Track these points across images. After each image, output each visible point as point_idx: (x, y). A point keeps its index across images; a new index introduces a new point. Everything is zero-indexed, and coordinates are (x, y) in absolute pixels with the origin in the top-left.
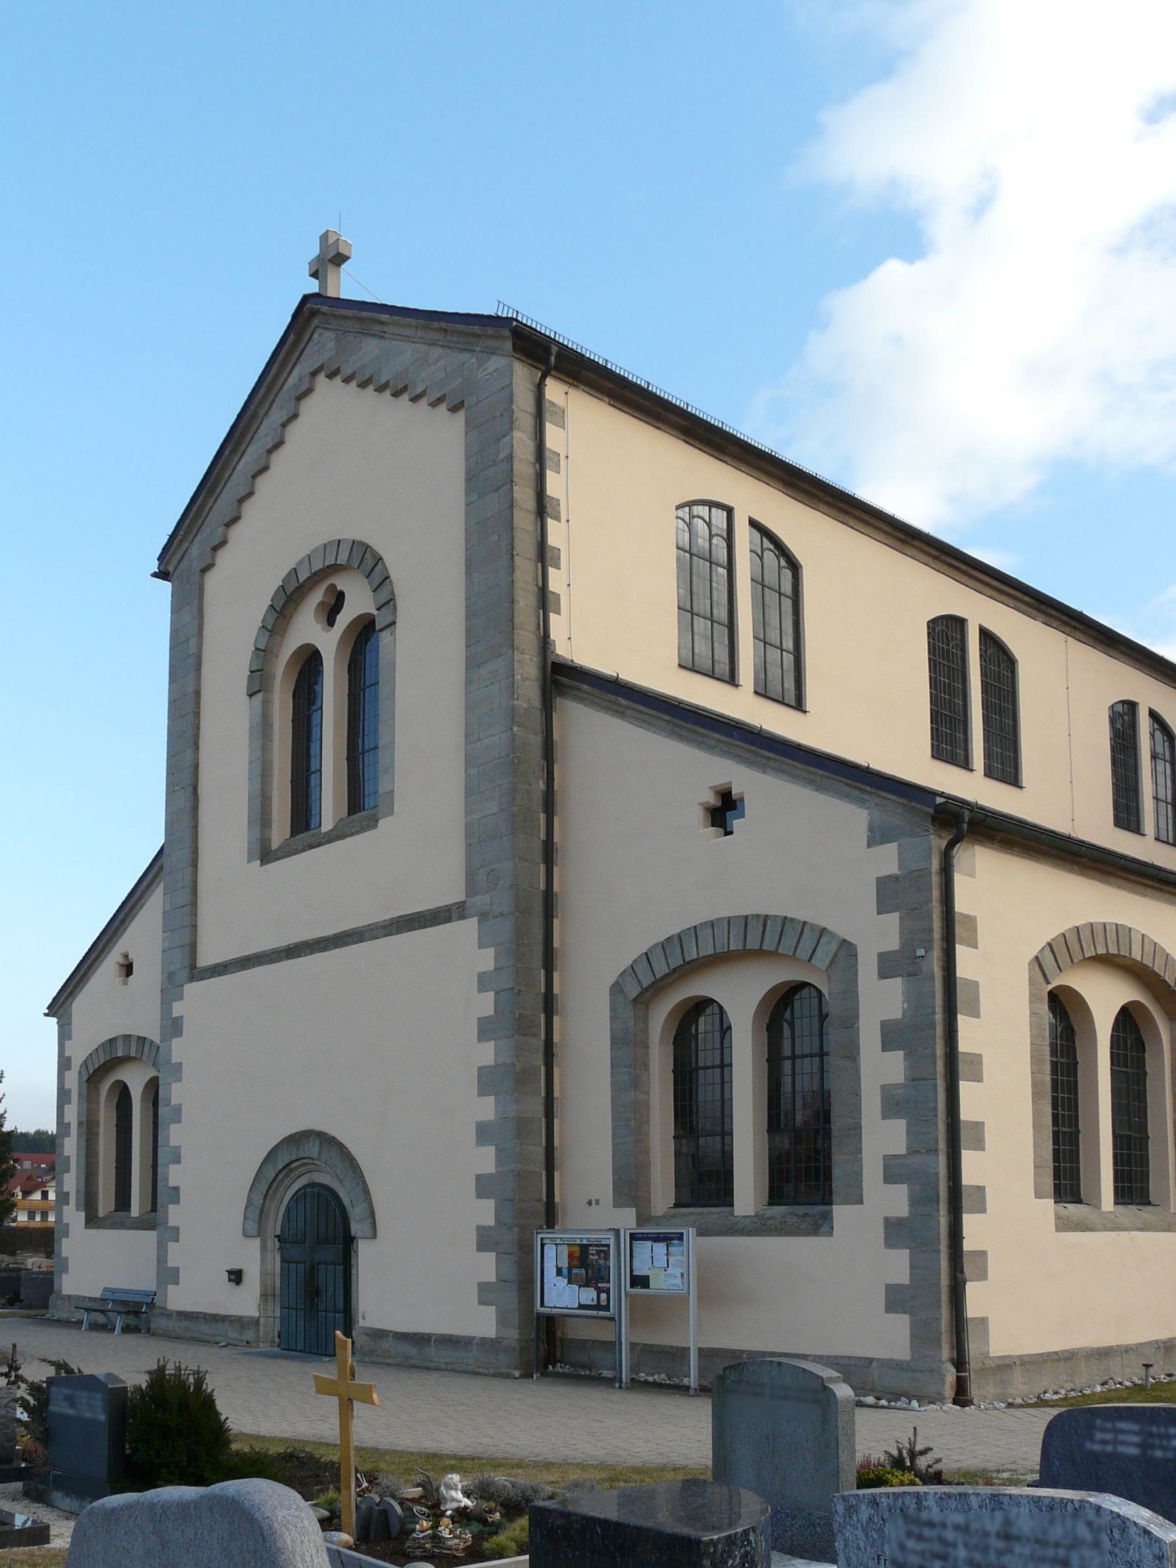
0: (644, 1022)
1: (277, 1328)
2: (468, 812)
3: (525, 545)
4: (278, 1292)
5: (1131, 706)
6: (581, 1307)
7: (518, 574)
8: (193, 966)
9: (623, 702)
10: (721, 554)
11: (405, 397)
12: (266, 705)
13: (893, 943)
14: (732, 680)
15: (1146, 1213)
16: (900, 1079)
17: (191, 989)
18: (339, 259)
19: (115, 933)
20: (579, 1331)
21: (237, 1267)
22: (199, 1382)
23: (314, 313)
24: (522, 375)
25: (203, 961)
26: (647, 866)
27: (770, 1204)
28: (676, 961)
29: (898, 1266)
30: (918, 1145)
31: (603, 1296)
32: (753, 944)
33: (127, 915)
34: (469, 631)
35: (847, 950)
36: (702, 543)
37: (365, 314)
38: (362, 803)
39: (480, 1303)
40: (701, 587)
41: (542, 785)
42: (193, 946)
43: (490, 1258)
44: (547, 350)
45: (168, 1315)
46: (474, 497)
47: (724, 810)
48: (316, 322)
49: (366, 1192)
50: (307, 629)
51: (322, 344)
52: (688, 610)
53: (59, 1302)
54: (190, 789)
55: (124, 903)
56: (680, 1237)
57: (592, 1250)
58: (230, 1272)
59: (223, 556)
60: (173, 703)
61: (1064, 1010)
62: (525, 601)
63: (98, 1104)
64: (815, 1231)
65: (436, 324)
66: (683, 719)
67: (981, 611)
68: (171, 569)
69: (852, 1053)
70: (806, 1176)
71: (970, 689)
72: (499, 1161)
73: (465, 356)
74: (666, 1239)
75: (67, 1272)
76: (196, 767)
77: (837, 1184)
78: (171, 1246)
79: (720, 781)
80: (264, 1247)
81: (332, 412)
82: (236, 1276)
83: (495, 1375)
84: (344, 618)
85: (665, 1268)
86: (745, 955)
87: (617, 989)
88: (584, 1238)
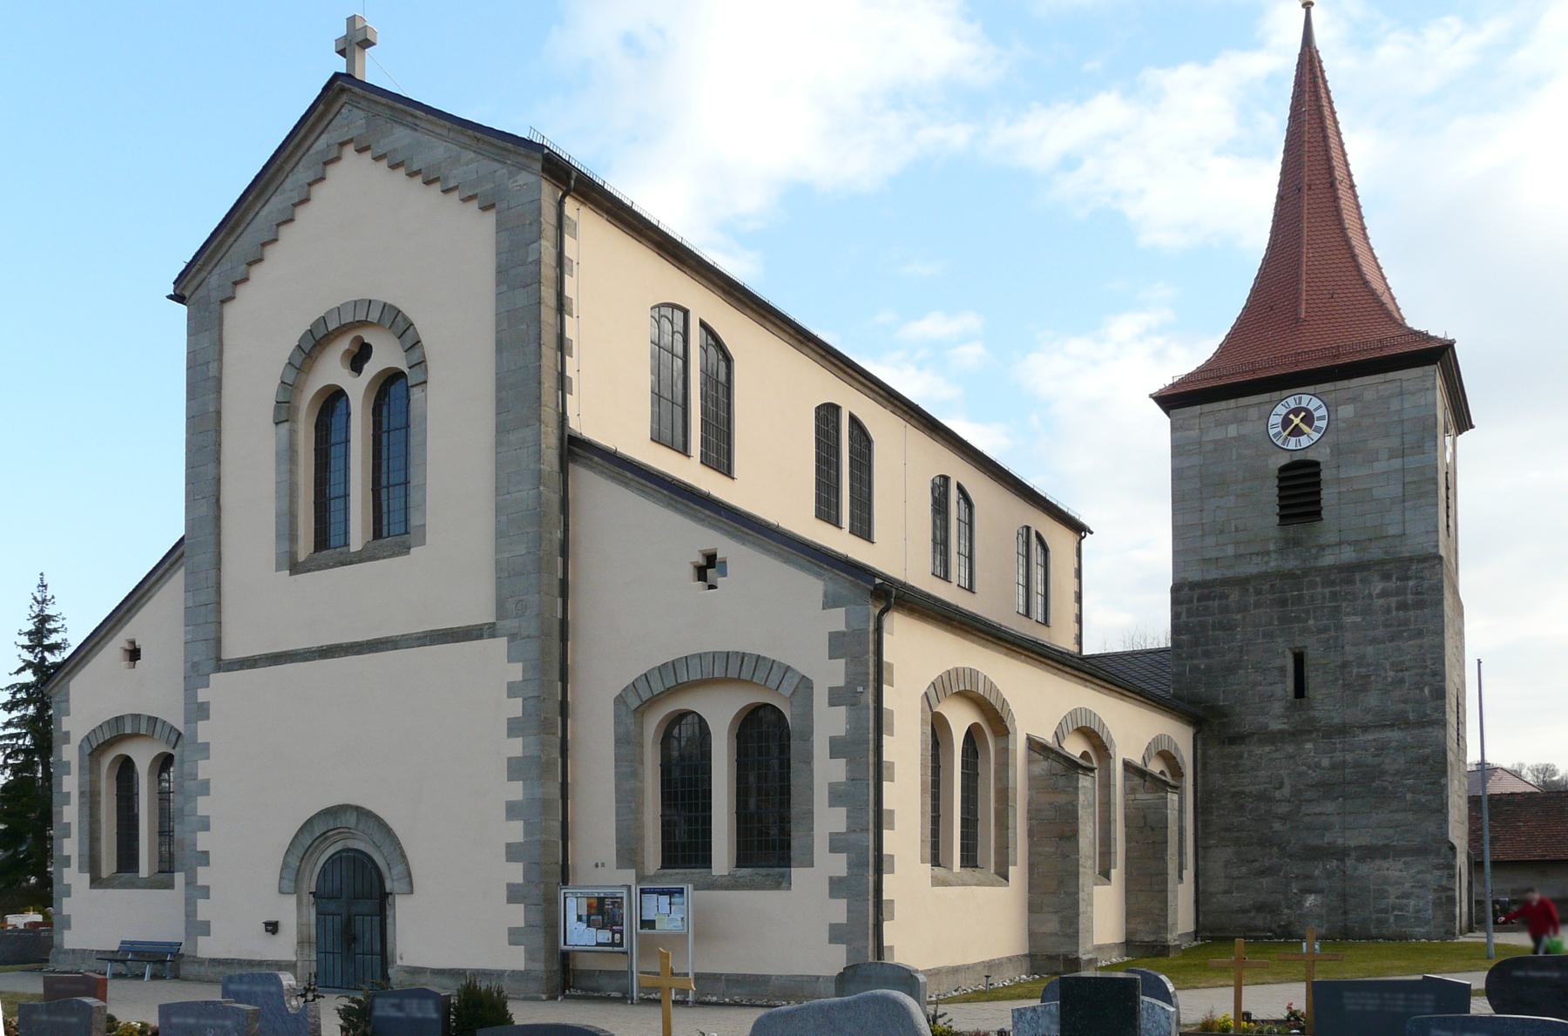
0: (640, 726)
1: (314, 969)
2: (498, 549)
3: (549, 337)
4: (313, 939)
5: (946, 479)
6: (598, 944)
7: (544, 360)
8: (219, 659)
9: (629, 475)
10: (679, 349)
11: (437, 187)
12: (293, 433)
13: (840, 681)
14: (685, 451)
15: (977, 873)
16: (844, 779)
17: (217, 679)
18: (366, 43)
19: (119, 621)
20: (582, 964)
21: (273, 919)
22: (499, 993)
23: (343, 90)
24: (548, 193)
25: (231, 652)
26: (644, 607)
27: (739, 865)
28: (671, 682)
29: (839, 911)
30: (855, 825)
31: (617, 936)
32: (733, 673)
33: (134, 605)
34: (499, 401)
35: (806, 684)
36: (667, 340)
37: (398, 105)
38: (393, 527)
39: (511, 943)
40: (665, 374)
41: (559, 535)
42: (218, 641)
43: (519, 909)
44: (569, 175)
45: (201, 962)
46: (505, 288)
47: (707, 568)
48: (344, 98)
49: (404, 856)
50: (332, 370)
51: (351, 120)
52: (657, 396)
53: (61, 956)
54: (213, 500)
55: (131, 594)
56: (681, 891)
57: (608, 901)
58: (267, 924)
59: (242, 291)
60: (191, 419)
61: (938, 729)
62: (549, 382)
63: (99, 776)
64: (777, 885)
65: (470, 132)
66: (679, 495)
67: (853, 402)
68: (187, 294)
69: (808, 760)
70: (769, 845)
71: (841, 459)
72: (526, 833)
73: (496, 165)
74: (670, 893)
75: (69, 928)
76: (219, 480)
77: (795, 852)
78: (201, 903)
79: (708, 547)
80: (299, 903)
81: (354, 183)
82: (272, 927)
83: (525, 999)
84: (372, 368)
85: (668, 916)
86: (725, 681)
87: (620, 700)
88: (601, 892)
